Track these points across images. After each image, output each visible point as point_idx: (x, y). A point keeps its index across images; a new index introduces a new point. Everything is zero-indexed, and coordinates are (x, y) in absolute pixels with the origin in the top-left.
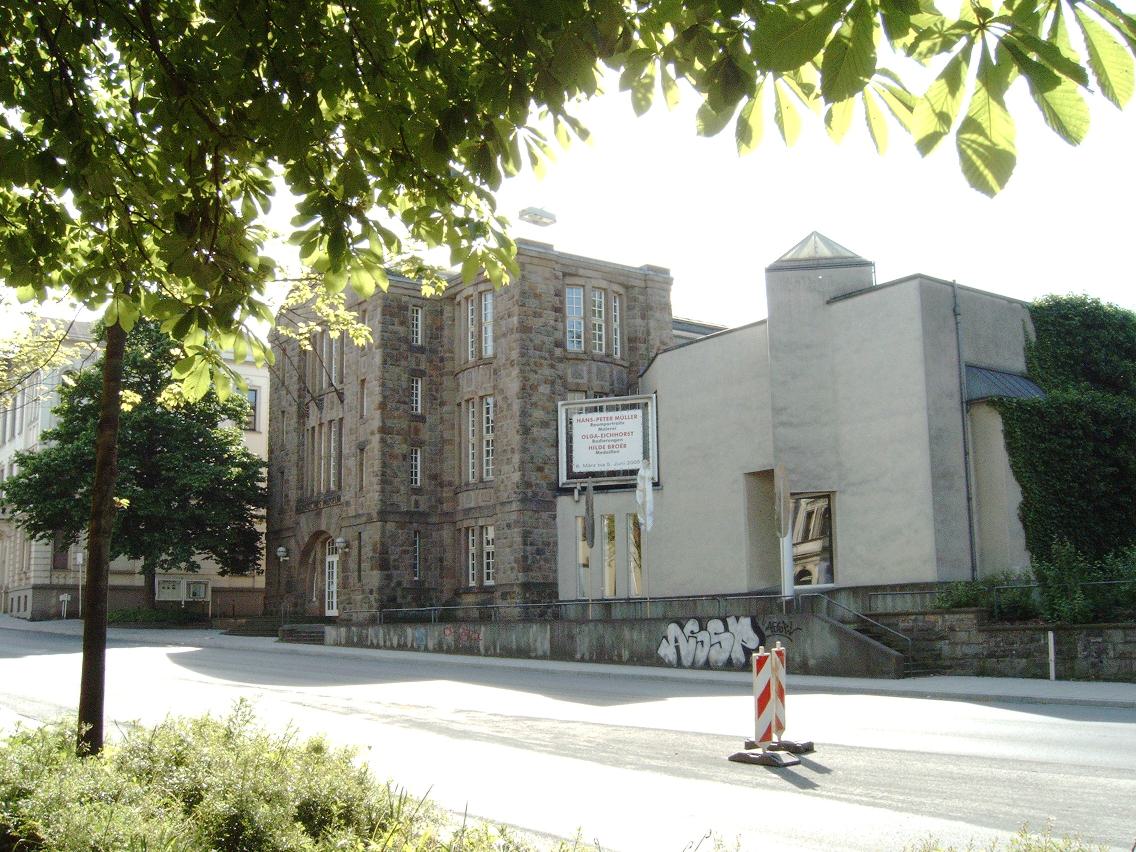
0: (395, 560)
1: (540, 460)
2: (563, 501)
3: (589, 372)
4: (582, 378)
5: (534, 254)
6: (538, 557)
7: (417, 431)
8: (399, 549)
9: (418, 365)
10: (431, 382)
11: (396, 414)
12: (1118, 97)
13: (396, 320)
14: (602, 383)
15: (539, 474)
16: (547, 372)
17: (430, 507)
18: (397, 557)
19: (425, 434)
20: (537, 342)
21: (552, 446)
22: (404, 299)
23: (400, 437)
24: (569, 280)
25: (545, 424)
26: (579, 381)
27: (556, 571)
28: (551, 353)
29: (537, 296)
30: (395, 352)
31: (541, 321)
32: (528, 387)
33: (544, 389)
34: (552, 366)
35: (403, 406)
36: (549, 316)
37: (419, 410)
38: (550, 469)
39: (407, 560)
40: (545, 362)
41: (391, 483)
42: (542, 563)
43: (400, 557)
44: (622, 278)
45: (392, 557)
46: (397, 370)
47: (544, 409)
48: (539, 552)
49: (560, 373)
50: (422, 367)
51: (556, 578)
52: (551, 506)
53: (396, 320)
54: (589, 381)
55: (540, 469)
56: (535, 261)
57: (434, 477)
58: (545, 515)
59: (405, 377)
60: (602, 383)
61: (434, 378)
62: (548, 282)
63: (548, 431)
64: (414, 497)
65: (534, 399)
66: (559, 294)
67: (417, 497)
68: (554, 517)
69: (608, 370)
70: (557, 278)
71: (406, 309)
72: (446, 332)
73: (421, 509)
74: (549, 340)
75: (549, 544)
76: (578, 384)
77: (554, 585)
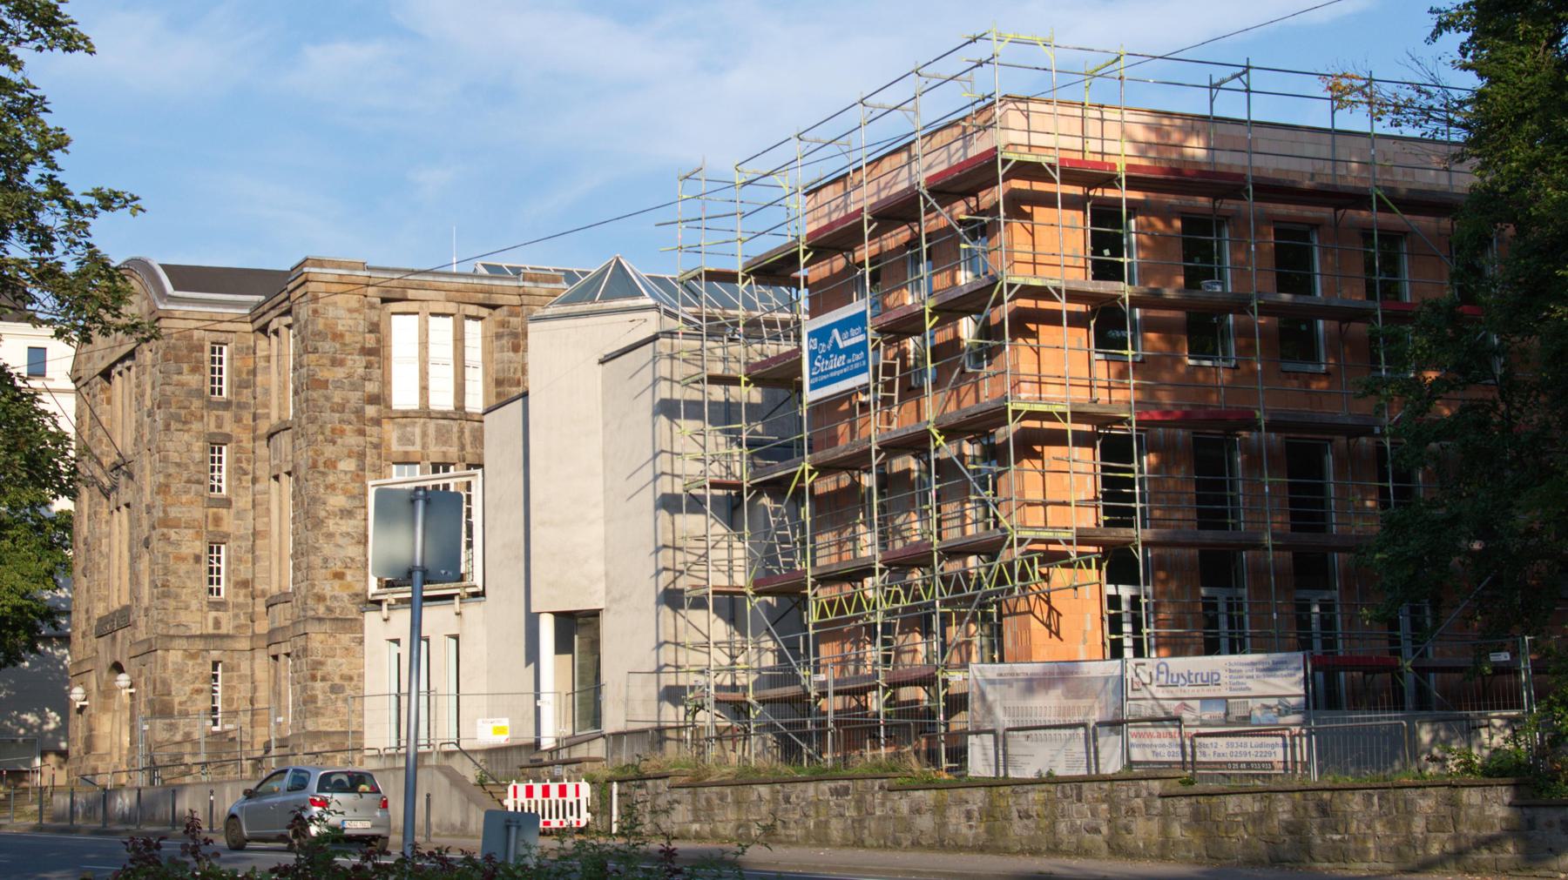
0: (181, 704)
1: (339, 564)
2: (372, 619)
3: (424, 434)
4: (413, 444)
5: (329, 278)
6: (333, 696)
7: (217, 520)
8: (188, 689)
9: (219, 426)
10: (240, 449)
11: (184, 498)
12: (74, 421)
13: (185, 367)
14: (444, 449)
15: (337, 583)
16: (352, 440)
17: (237, 627)
18: (184, 698)
19: (229, 523)
20: (337, 399)
21: (359, 543)
22: (196, 334)
23: (191, 531)
24: (394, 307)
25: (347, 513)
26: (410, 448)
27: (362, 716)
28: (359, 413)
29: (337, 336)
30: (183, 412)
31: (340, 373)
32: (321, 464)
33: (348, 465)
34: (362, 433)
35: (194, 487)
36: (357, 364)
37: (224, 491)
38: (353, 576)
39: (203, 703)
40: (348, 428)
41: (177, 596)
42: (340, 704)
43: (190, 698)
44: (481, 295)
45: (177, 700)
46: (186, 437)
47: (345, 492)
48: (335, 689)
49: (375, 440)
50: (227, 429)
51: (362, 725)
52: (352, 625)
53: (185, 367)
54: (423, 448)
55: (339, 576)
56: (335, 288)
57: (244, 584)
58: (345, 638)
59: (198, 446)
60: (444, 449)
61: (244, 444)
62: (356, 315)
63: (352, 522)
64: (213, 614)
65: (331, 479)
66: (374, 328)
67: (220, 614)
68: (361, 642)
69: (455, 429)
70: (372, 306)
71: (201, 349)
72: (259, 378)
73: (223, 631)
74: (355, 397)
75: (351, 678)
76: (406, 453)
77: (359, 734)
